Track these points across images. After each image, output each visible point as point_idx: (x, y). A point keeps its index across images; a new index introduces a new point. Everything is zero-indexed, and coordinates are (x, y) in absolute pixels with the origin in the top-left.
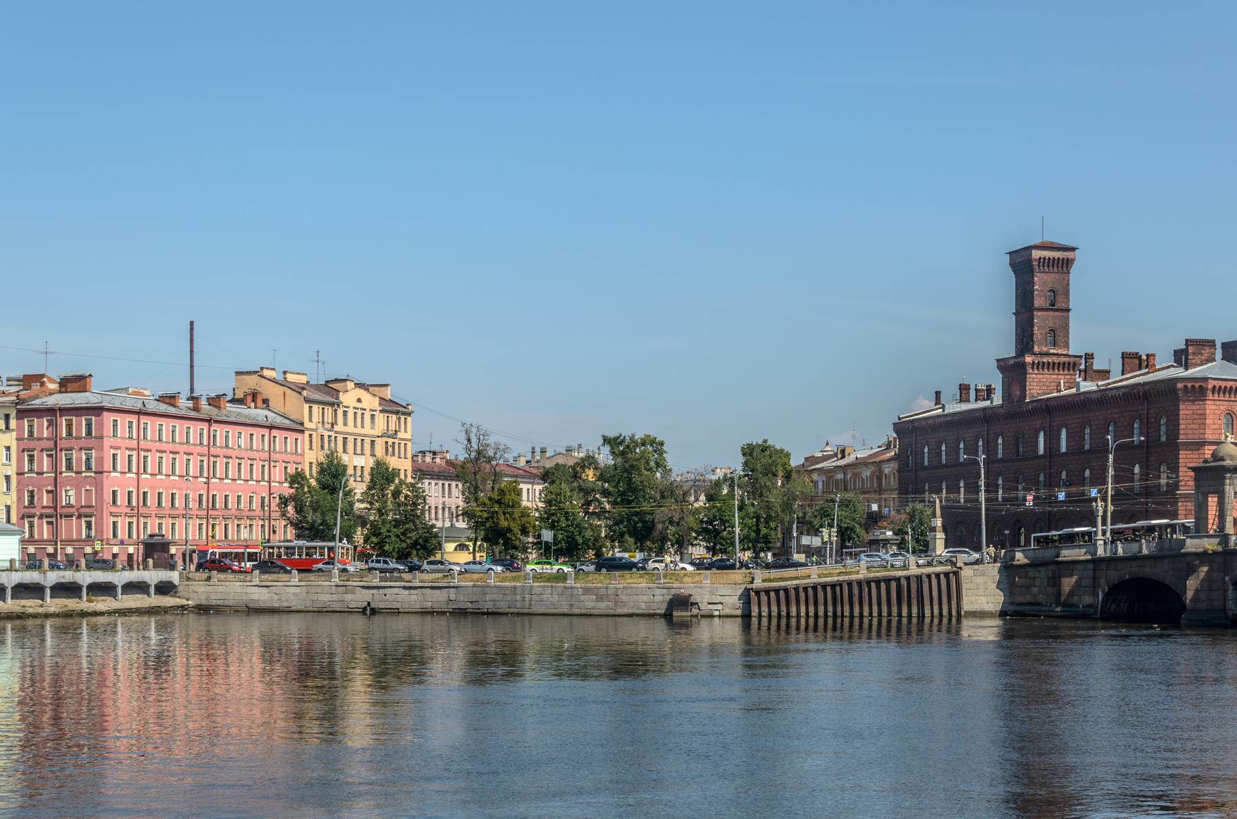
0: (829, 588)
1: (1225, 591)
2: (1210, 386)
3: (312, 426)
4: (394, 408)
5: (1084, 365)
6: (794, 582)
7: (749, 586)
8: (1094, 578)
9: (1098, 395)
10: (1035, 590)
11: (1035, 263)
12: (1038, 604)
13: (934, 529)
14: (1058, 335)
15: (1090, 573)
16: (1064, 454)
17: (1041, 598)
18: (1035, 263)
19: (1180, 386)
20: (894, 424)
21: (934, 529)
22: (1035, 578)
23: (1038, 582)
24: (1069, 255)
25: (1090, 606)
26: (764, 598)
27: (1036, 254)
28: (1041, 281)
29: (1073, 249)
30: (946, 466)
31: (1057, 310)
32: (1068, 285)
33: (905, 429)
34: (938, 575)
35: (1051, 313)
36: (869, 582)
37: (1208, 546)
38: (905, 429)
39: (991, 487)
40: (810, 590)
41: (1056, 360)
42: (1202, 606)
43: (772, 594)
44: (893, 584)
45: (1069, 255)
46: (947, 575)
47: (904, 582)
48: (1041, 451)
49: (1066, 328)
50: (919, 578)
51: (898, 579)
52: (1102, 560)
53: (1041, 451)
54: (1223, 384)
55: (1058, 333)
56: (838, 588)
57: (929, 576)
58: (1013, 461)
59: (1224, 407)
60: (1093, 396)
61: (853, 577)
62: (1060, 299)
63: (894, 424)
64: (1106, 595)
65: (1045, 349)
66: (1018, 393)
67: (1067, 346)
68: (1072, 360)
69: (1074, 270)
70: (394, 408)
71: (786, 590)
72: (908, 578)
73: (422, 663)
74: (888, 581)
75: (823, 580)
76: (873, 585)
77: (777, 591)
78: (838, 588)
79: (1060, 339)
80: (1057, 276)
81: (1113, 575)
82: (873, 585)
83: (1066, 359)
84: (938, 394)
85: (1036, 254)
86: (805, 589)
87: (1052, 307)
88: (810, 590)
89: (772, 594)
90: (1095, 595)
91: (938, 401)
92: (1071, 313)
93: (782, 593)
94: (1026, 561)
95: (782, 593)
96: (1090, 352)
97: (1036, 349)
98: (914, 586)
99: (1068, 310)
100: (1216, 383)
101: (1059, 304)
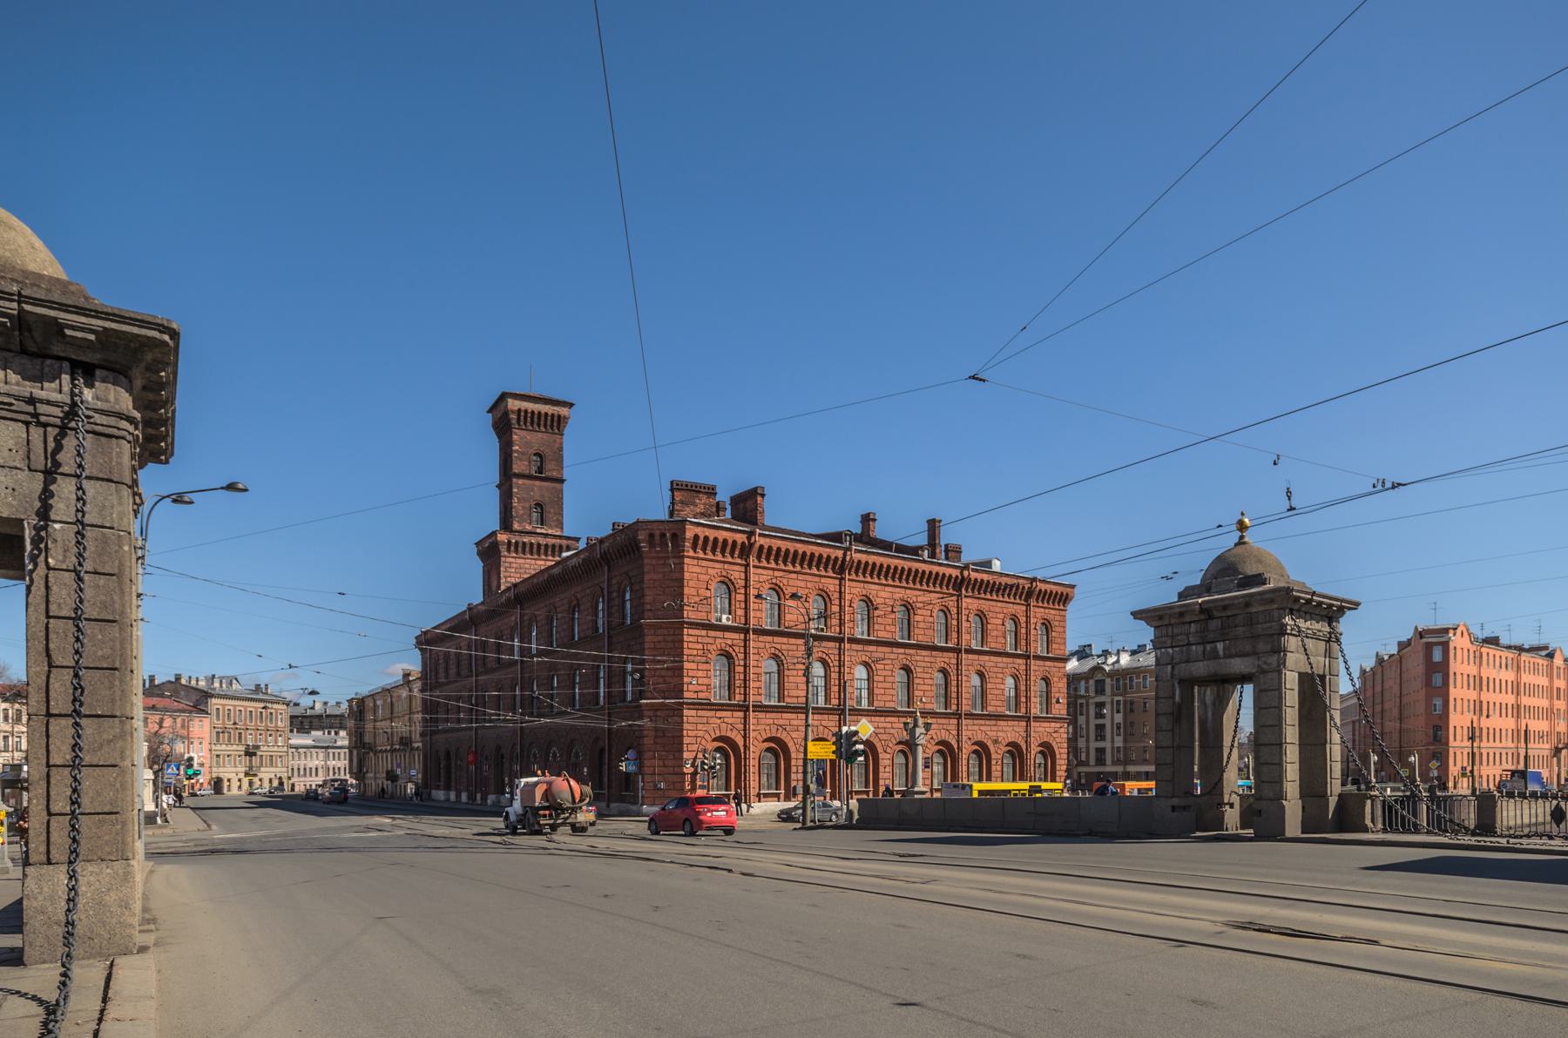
3: (1457, 743)
4: (313, 693)
11: (513, 417)
18: (513, 417)
24: (564, 411)
29: (571, 405)
32: (561, 449)
33: (426, 641)
35: (537, 483)
38: (426, 641)
39: (609, 685)
41: (543, 541)
45: (564, 411)
55: (547, 508)
59: (715, 570)
60: (555, 571)
65: (529, 528)
67: (560, 525)
69: (568, 431)
70: (313, 693)
80: (545, 436)
85: (513, 404)
87: (540, 475)
97: (516, 526)
99: (562, 481)
101: (547, 470)
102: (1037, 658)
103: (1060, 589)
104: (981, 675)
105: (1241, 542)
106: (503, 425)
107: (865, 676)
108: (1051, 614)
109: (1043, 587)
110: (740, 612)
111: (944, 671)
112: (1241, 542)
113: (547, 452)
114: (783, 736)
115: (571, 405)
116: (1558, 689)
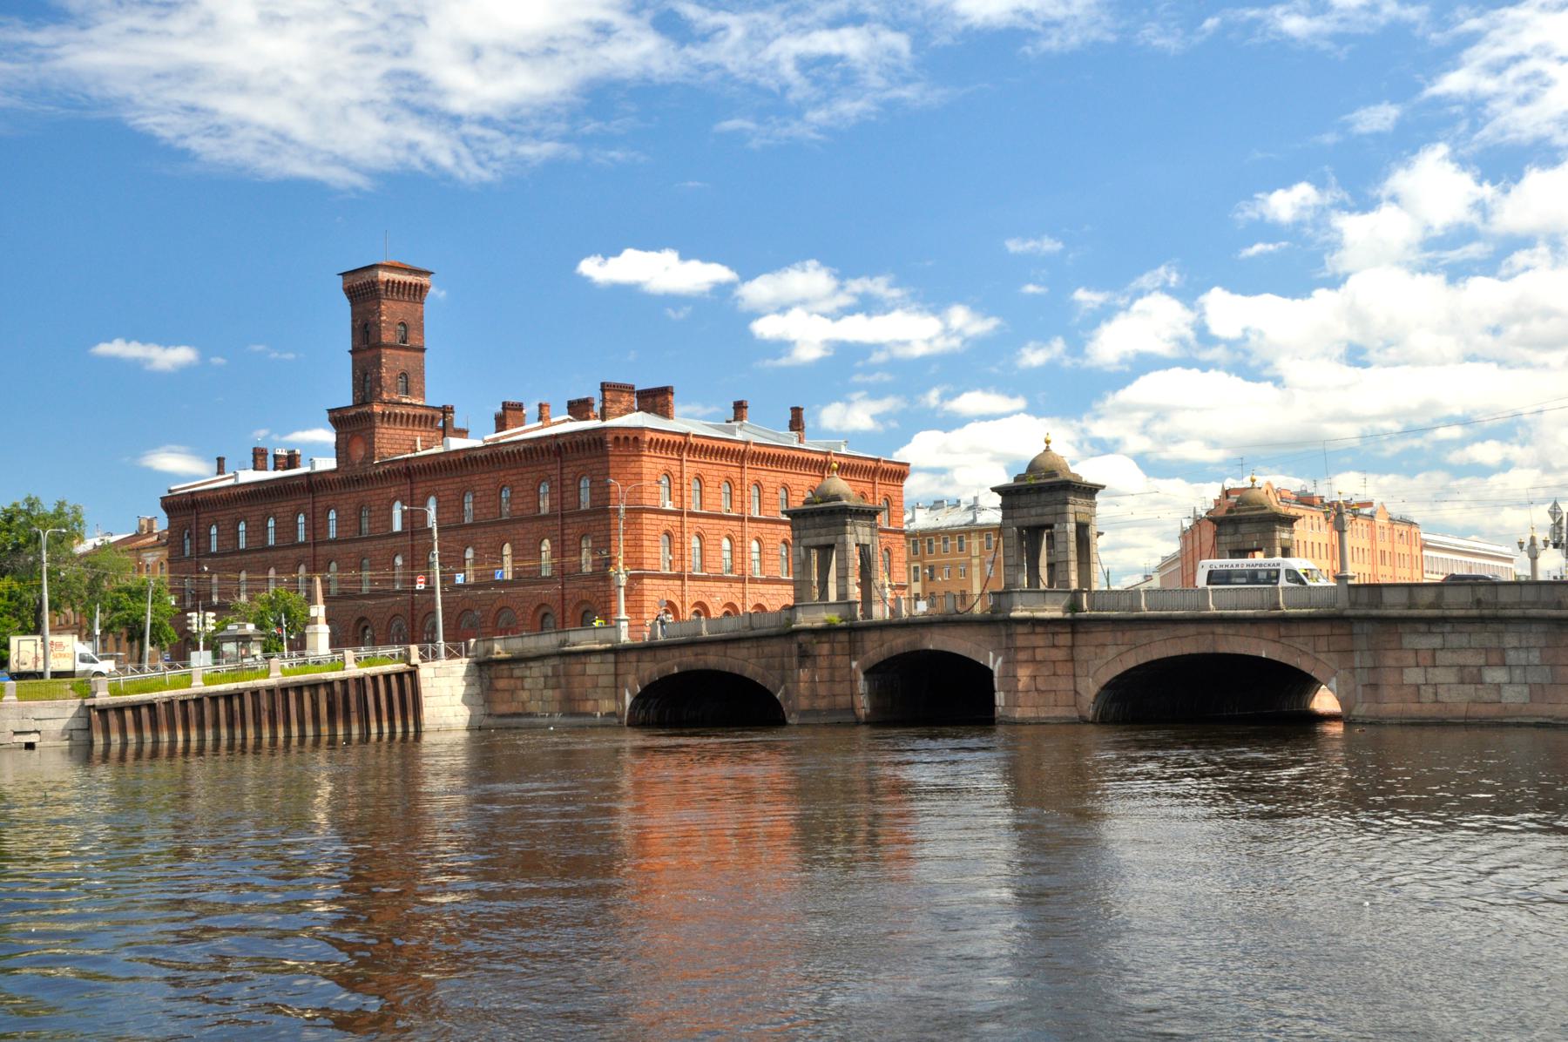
0: (222, 702)
1: (853, 682)
2: (647, 439)
5: (441, 420)
6: (166, 693)
7: (89, 702)
8: (616, 675)
9: (488, 452)
10: (524, 695)
12: (530, 715)
13: (314, 621)
14: (409, 381)
15: (611, 668)
16: (398, 534)
17: (533, 706)
19: (610, 438)
20: (163, 498)
21: (314, 621)
22: (522, 678)
23: (528, 683)
24: (424, 280)
25: (612, 714)
26: (113, 719)
27: (384, 276)
28: (390, 312)
29: (428, 273)
30: (245, 552)
31: (407, 349)
32: (422, 318)
34: (387, 676)
36: (285, 689)
37: (1519, 572)
40: (191, 705)
41: (412, 411)
42: (822, 704)
43: (129, 714)
44: (323, 693)
45: (424, 280)
46: (400, 675)
47: (338, 687)
48: (397, 526)
49: (420, 372)
50: (360, 681)
51: (329, 684)
52: (627, 649)
53: (397, 526)
54: (661, 437)
55: (411, 377)
56: (236, 702)
57: (374, 678)
58: (258, 551)
59: (661, 464)
60: (479, 453)
61: (261, 682)
62: (413, 335)
63: (163, 498)
64: (637, 698)
65: (396, 397)
66: (361, 453)
67: (422, 395)
68: (429, 413)
71: (151, 706)
72: (344, 682)
73: (607, 871)
74: (314, 686)
75: (213, 688)
76: (292, 695)
77: (136, 708)
78: (236, 702)
79: (414, 385)
80: (408, 306)
81: (651, 670)
82: (292, 695)
83: (423, 412)
84: (220, 461)
86: (184, 703)
87: (403, 344)
88: (191, 705)
89: (129, 714)
90: (619, 698)
91: (221, 470)
92: (426, 354)
93: (144, 711)
94: (503, 655)
95: (144, 711)
96: (449, 403)
97: (385, 396)
98: (353, 693)
99: (423, 350)
100: (655, 436)
102: (691, 514)
103: (898, 467)
104: (699, 536)
105: (1047, 450)
106: (353, 293)
107: (698, 545)
108: (891, 490)
109: (886, 466)
110: (678, 499)
111: (668, 533)
112: (1047, 450)
113: (410, 320)
114: (704, 600)
115: (428, 273)
116: (1383, 553)
